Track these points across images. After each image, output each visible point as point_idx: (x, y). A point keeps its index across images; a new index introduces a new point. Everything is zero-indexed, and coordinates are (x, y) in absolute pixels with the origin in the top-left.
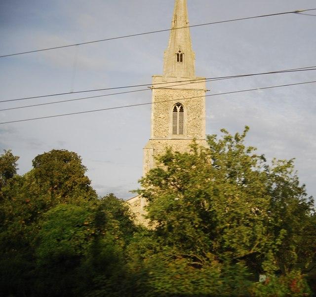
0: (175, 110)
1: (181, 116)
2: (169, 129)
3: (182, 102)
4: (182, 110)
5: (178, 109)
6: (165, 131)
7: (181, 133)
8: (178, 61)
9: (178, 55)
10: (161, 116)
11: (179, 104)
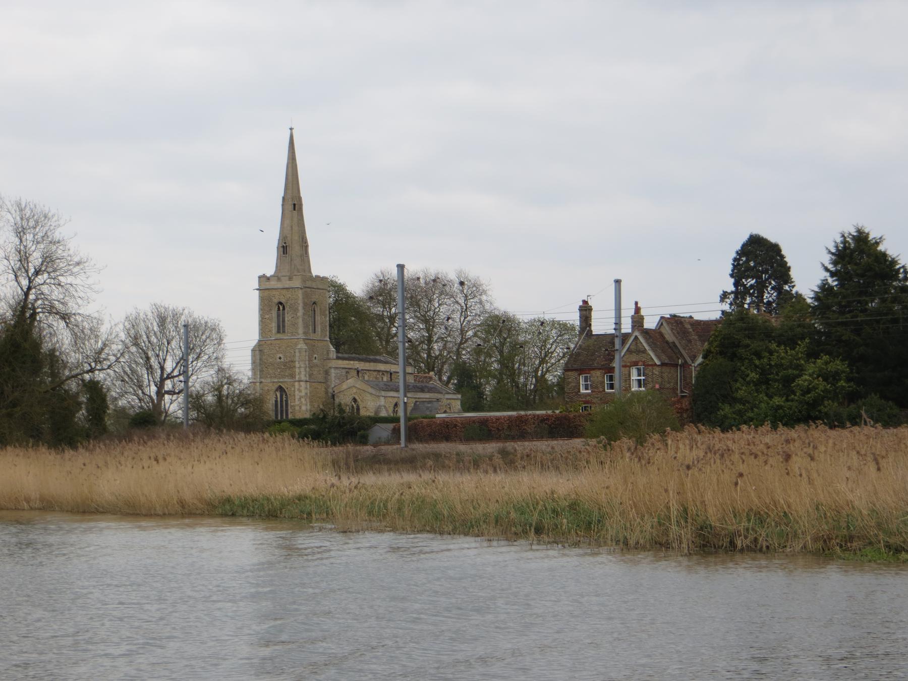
0: (279, 308)
1: (284, 314)
3: (283, 301)
4: (284, 309)
5: (281, 308)
6: (270, 331)
7: (284, 332)
8: (284, 254)
9: (283, 247)
10: (267, 316)
11: (281, 303)
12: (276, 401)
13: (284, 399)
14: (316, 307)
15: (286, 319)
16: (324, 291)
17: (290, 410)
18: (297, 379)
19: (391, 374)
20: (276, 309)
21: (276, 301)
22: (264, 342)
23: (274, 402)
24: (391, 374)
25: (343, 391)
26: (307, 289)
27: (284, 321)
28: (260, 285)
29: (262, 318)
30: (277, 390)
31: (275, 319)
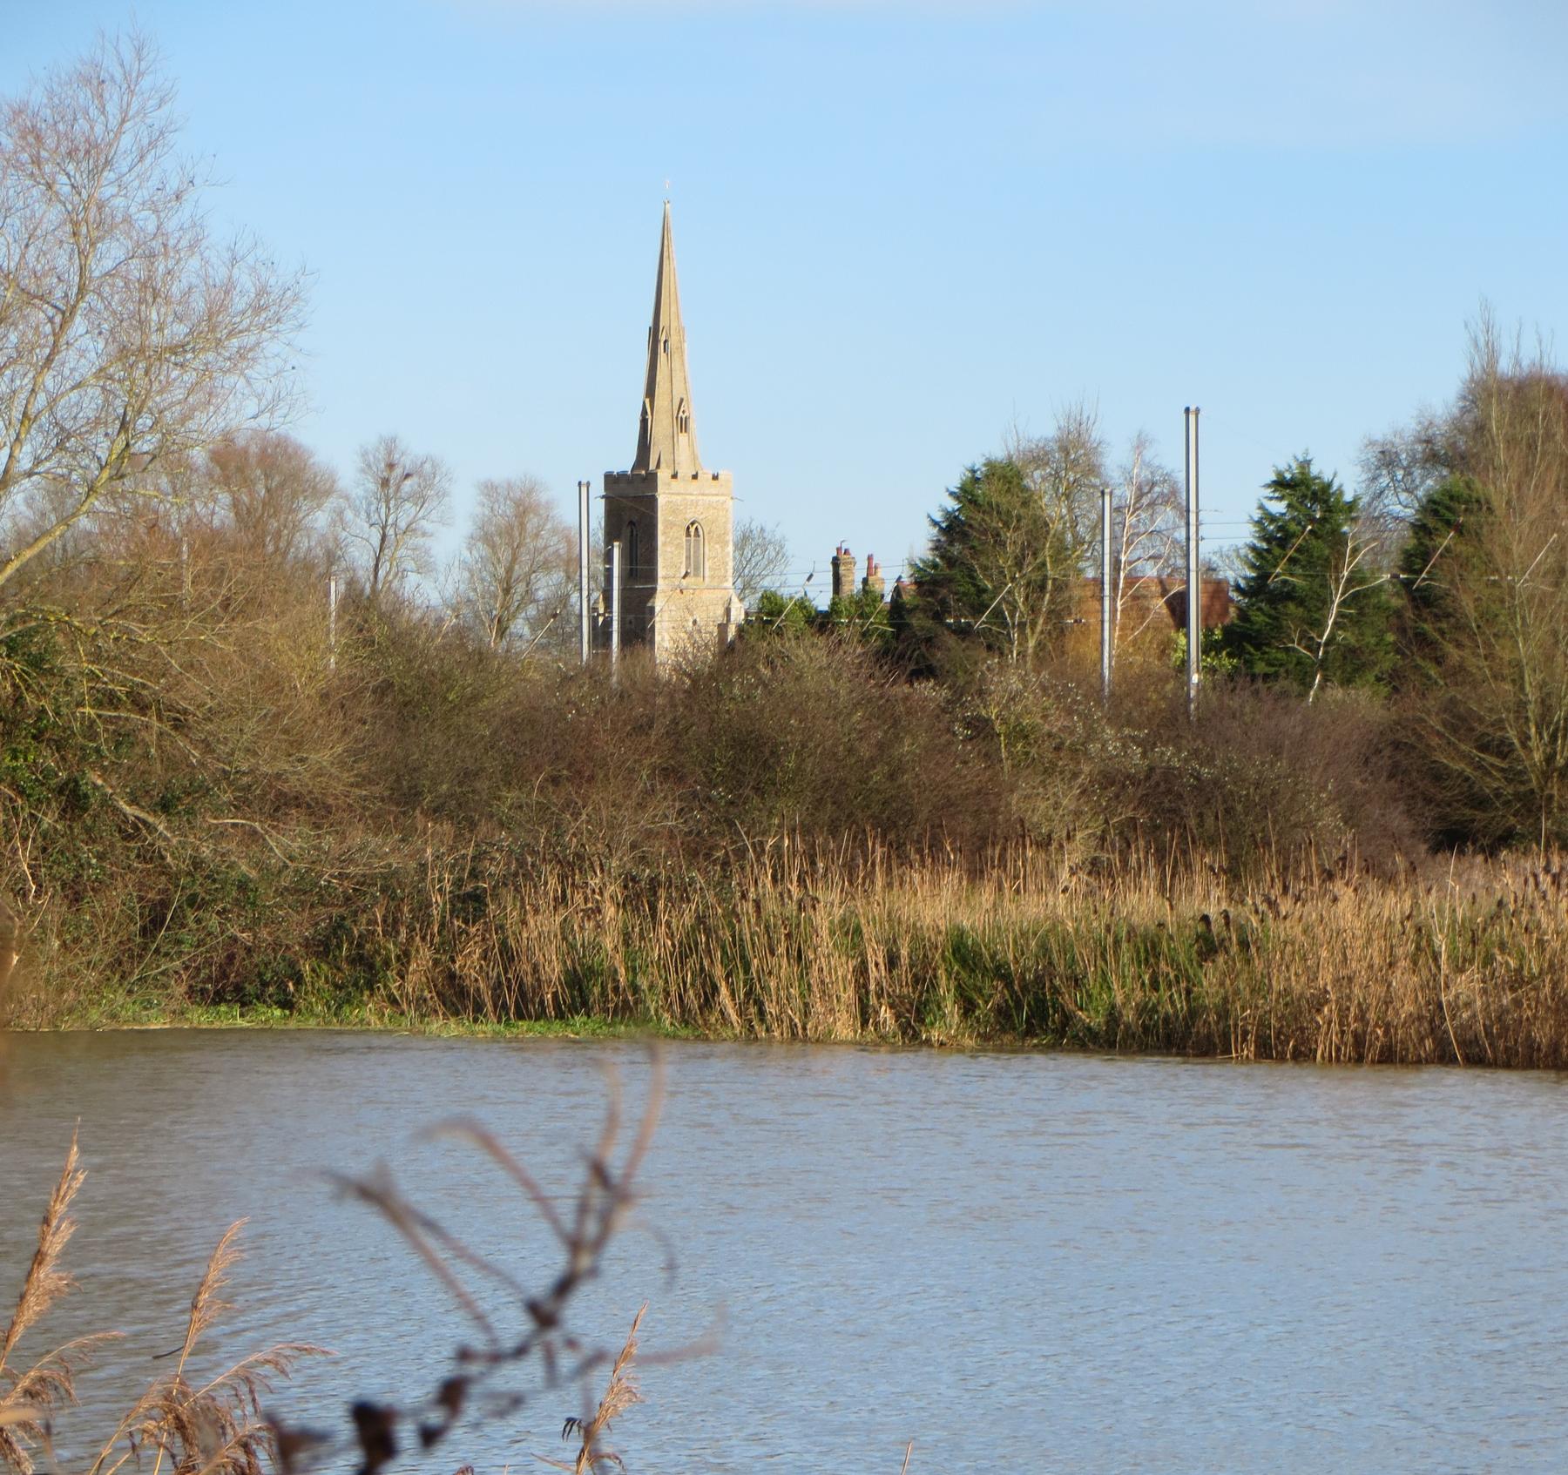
26: (674, 498)
28: (606, 489)
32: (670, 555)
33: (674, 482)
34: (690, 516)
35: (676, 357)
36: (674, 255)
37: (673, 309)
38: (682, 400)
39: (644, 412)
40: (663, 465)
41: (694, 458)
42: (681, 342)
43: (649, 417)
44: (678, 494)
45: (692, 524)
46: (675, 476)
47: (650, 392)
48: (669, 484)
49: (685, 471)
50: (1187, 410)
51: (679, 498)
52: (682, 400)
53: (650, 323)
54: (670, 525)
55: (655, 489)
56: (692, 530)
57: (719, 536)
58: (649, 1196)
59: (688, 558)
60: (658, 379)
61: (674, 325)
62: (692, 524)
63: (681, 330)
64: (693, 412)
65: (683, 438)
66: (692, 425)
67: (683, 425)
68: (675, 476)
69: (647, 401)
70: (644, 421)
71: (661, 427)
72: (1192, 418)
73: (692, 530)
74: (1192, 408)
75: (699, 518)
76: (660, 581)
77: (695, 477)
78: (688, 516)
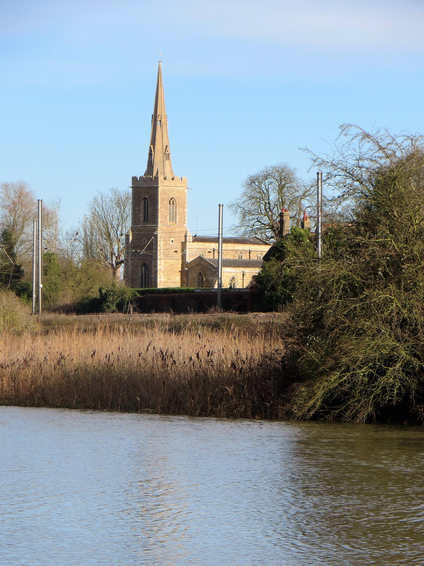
1: (148, 207)
2: (141, 218)
10: (137, 208)
12: (142, 274)
13: (147, 273)
14: (174, 201)
15: (149, 210)
16: (183, 188)
17: (150, 282)
18: (154, 258)
19: (250, 253)
20: (144, 203)
21: (143, 196)
22: (134, 228)
23: (140, 275)
24: (250, 253)
25: (193, 267)
26: (165, 188)
27: (148, 213)
28: (133, 184)
29: (134, 210)
30: (142, 266)
31: (142, 211)
32: (163, 212)
33: (165, 181)
34: (171, 196)
35: (164, 128)
36: (163, 84)
37: (163, 107)
38: (167, 146)
39: (151, 151)
40: (159, 174)
41: (172, 173)
42: (166, 121)
43: (153, 153)
44: (166, 186)
45: (171, 199)
46: (165, 179)
47: (153, 142)
48: (163, 182)
49: (169, 177)
50: (220, 205)
51: (167, 188)
52: (167, 146)
53: (152, 113)
54: (163, 199)
55: (157, 183)
56: (171, 202)
57: (182, 204)
58: (294, 442)
59: (170, 214)
60: (157, 136)
61: (163, 114)
62: (171, 199)
63: (166, 116)
64: (171, 150)
65: (167, 162)
66: (171, 156)
67: (167, 156)
68: (165, 179)
69: (152, 146)
70: (150, 155)
71: (158, 157)
72: (221, 207)
73: (171, 202)
74: (221, 205)
75: (174, 196)
76: (159, 223)
77: (173, 179)
78: (170, 196)
